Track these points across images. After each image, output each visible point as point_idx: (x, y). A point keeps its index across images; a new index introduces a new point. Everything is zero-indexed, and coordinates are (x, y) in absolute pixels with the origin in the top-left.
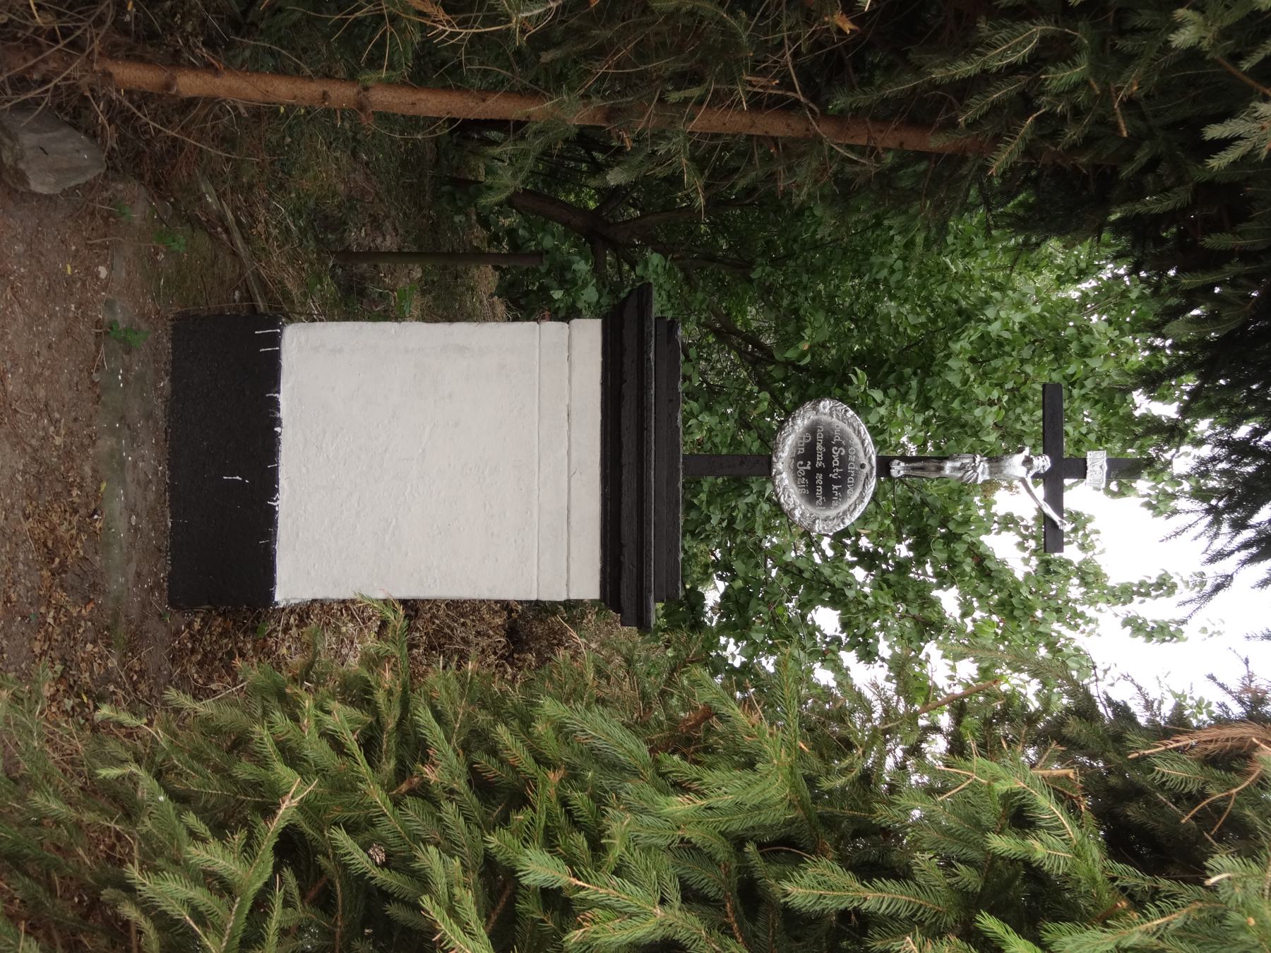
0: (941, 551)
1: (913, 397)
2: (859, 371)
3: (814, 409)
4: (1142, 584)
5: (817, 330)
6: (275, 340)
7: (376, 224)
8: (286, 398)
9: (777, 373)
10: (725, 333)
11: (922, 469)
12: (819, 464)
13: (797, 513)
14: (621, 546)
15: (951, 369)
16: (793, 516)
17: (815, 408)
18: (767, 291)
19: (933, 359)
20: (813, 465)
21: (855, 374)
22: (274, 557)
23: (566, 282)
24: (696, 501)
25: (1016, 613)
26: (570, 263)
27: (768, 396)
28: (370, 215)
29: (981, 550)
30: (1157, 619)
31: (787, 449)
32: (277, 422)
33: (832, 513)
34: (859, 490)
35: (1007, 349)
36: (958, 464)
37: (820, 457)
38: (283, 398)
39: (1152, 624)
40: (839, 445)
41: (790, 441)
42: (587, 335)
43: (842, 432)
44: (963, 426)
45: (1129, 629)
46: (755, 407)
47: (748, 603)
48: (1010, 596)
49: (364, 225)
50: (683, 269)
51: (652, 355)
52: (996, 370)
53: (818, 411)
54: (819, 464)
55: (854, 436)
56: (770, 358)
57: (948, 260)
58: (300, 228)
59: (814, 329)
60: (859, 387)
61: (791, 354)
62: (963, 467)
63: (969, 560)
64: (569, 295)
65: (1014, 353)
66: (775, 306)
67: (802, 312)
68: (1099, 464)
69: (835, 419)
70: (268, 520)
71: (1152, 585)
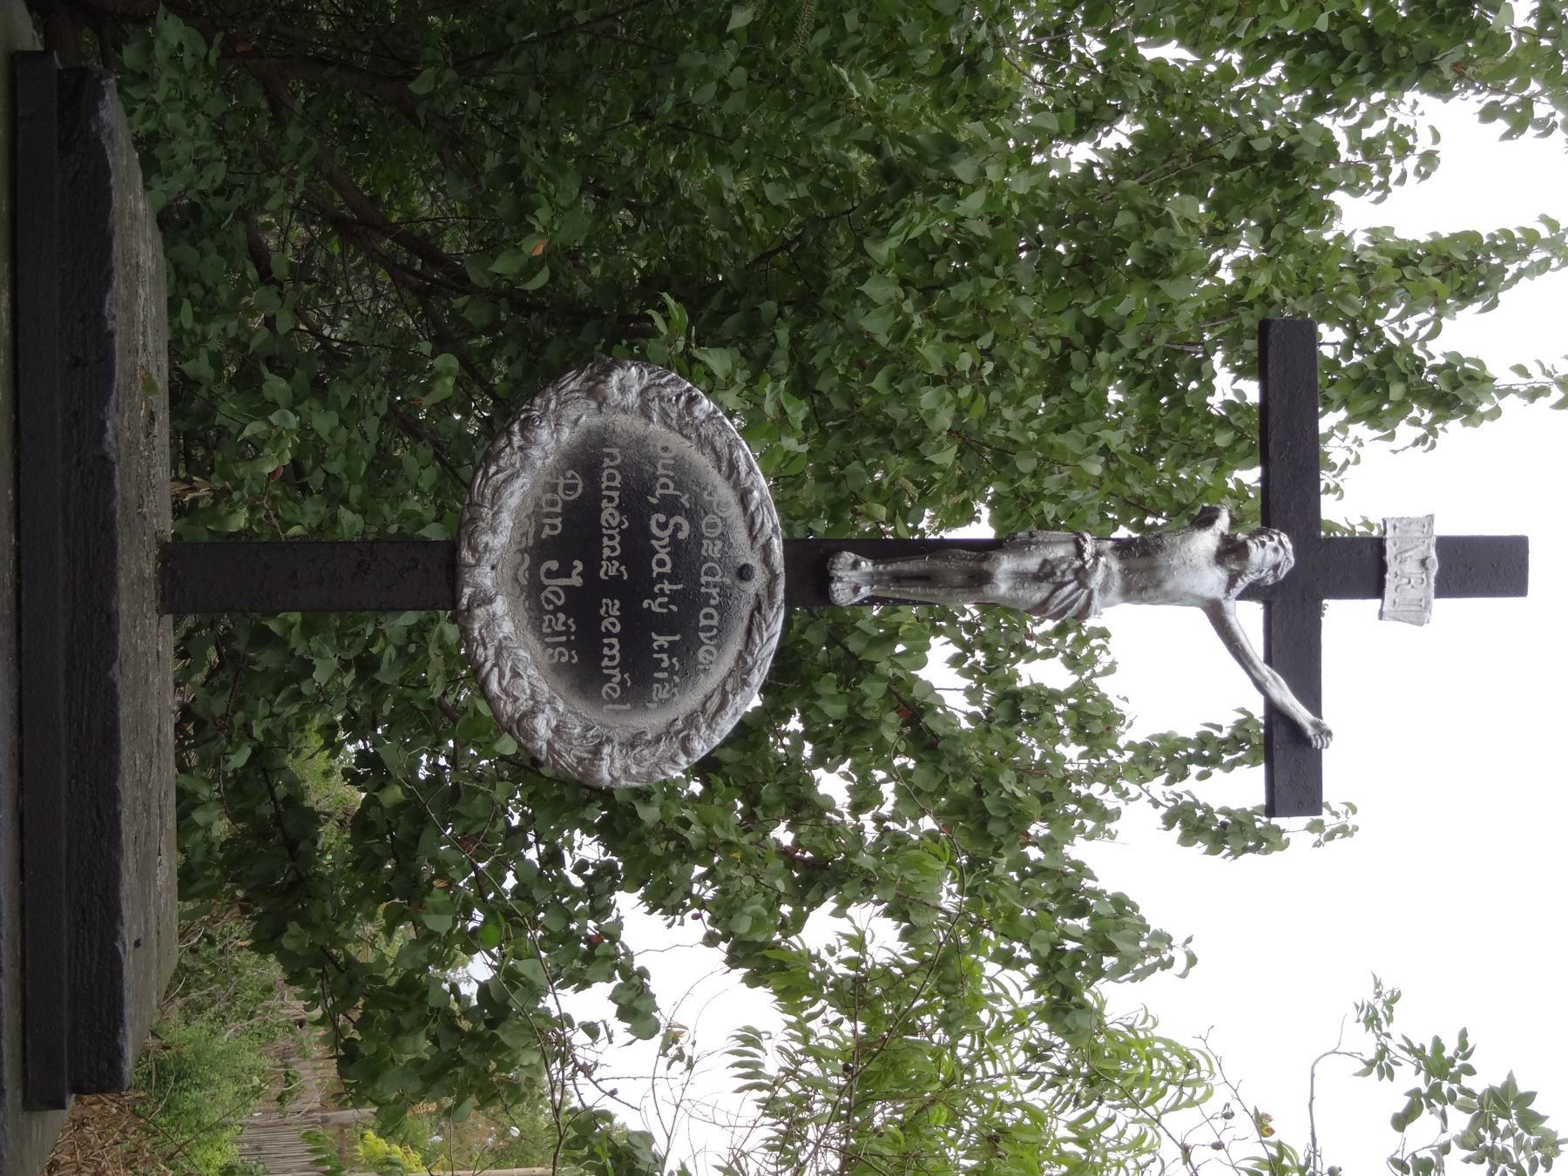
0: (833, 699)
1: (782, 366)
2: (671, 302)
3: (591, 393)
4: (1204, 740)
5: (556, 221)
9: (476, 314)
10: (358, 227)
11: (925, 578)
12: (609, 569)
13: (542, 726)
15: (869, 303)
16: (531, 735)
17: (593, 392)
18: (455, 141)
19: (823, 281)
20: (590, 573)
21: (663, 308)
24: (273, 626)
25: (994, 828)
27: (453, 362)
29: (916, 693)
30: (1234, 807)
31: (506, 521)
33: (651, 721)
34: (735, 645)
35: (984, 259)
36: (1032, 564)
37: (611, 547)
39: (1221, 818)
40: (670, 506)
41: (516, 496)
43: (680, 468)
44: (884, 431)
45: (1177, 831)
46: (426, 390)
47: (417, 838)
48: (978, 791)
52: (957, 306)
53: (602, 402)
54: (609, 569)
55: (717, 480)
56: (460, 282)
57: (844, 73)
59: (558, 211)
60: (671, 342)
61: (504, 265)
62: (1046, 573)
63: (892, 717)
65: (999, 270)
66: (470, 171)
67: (528, 173)
68: (1416, 555)
69: (656, 427)
71: (1224, 742)
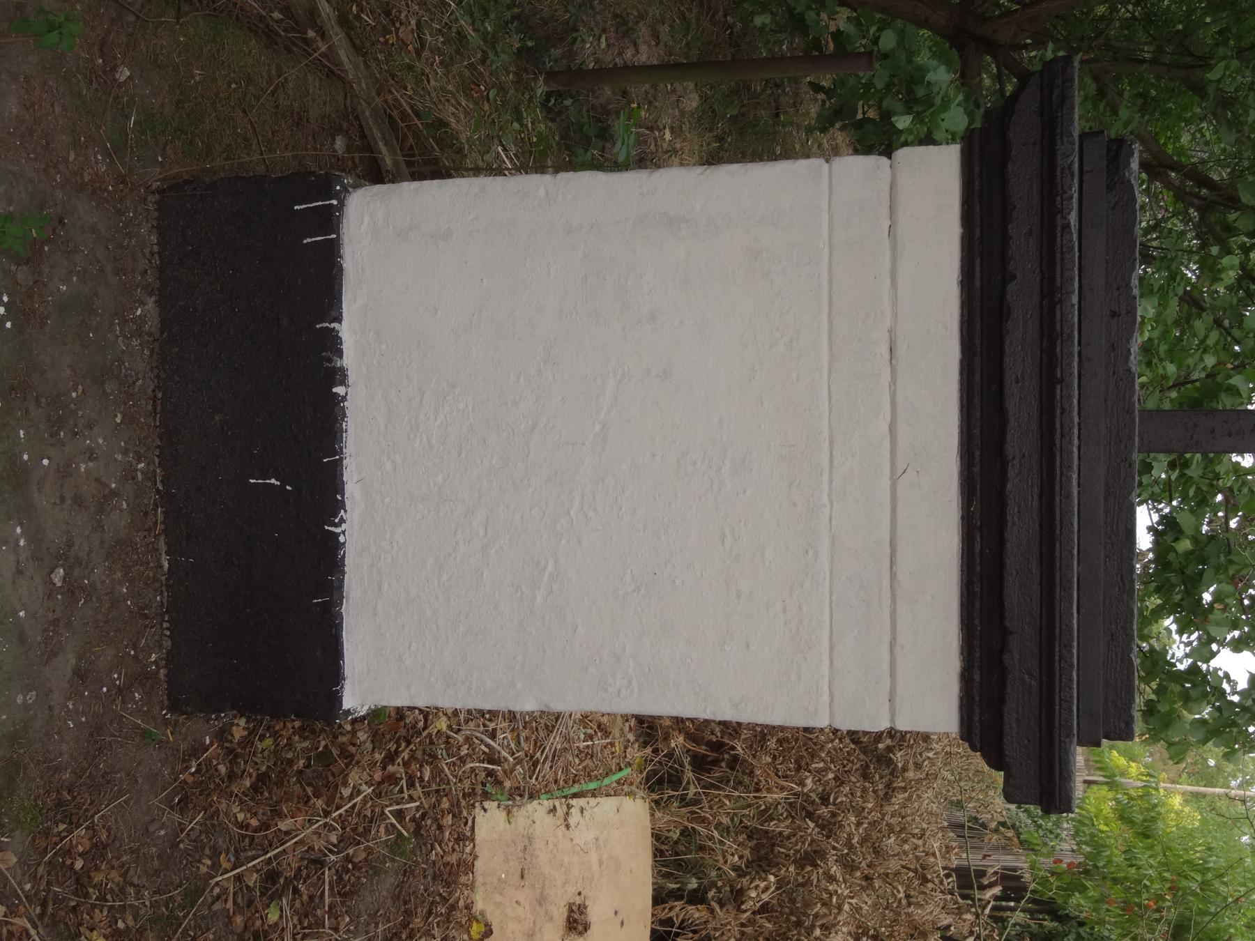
6: (329, 221)
7: (624, 29)
8: (350, 331)
14: (1005, 632)
22: (339, 627)
23: (917, 101)
26: (923, 70)
28: (616, 16)
32: (339, 376)
38: (347, 330)
42: (932, 179)
49: (604, 31)
50: (1096, 78)
51: (1073, 218)
58: (484, 35)
64: (922, 122)
70: (328, 556)
